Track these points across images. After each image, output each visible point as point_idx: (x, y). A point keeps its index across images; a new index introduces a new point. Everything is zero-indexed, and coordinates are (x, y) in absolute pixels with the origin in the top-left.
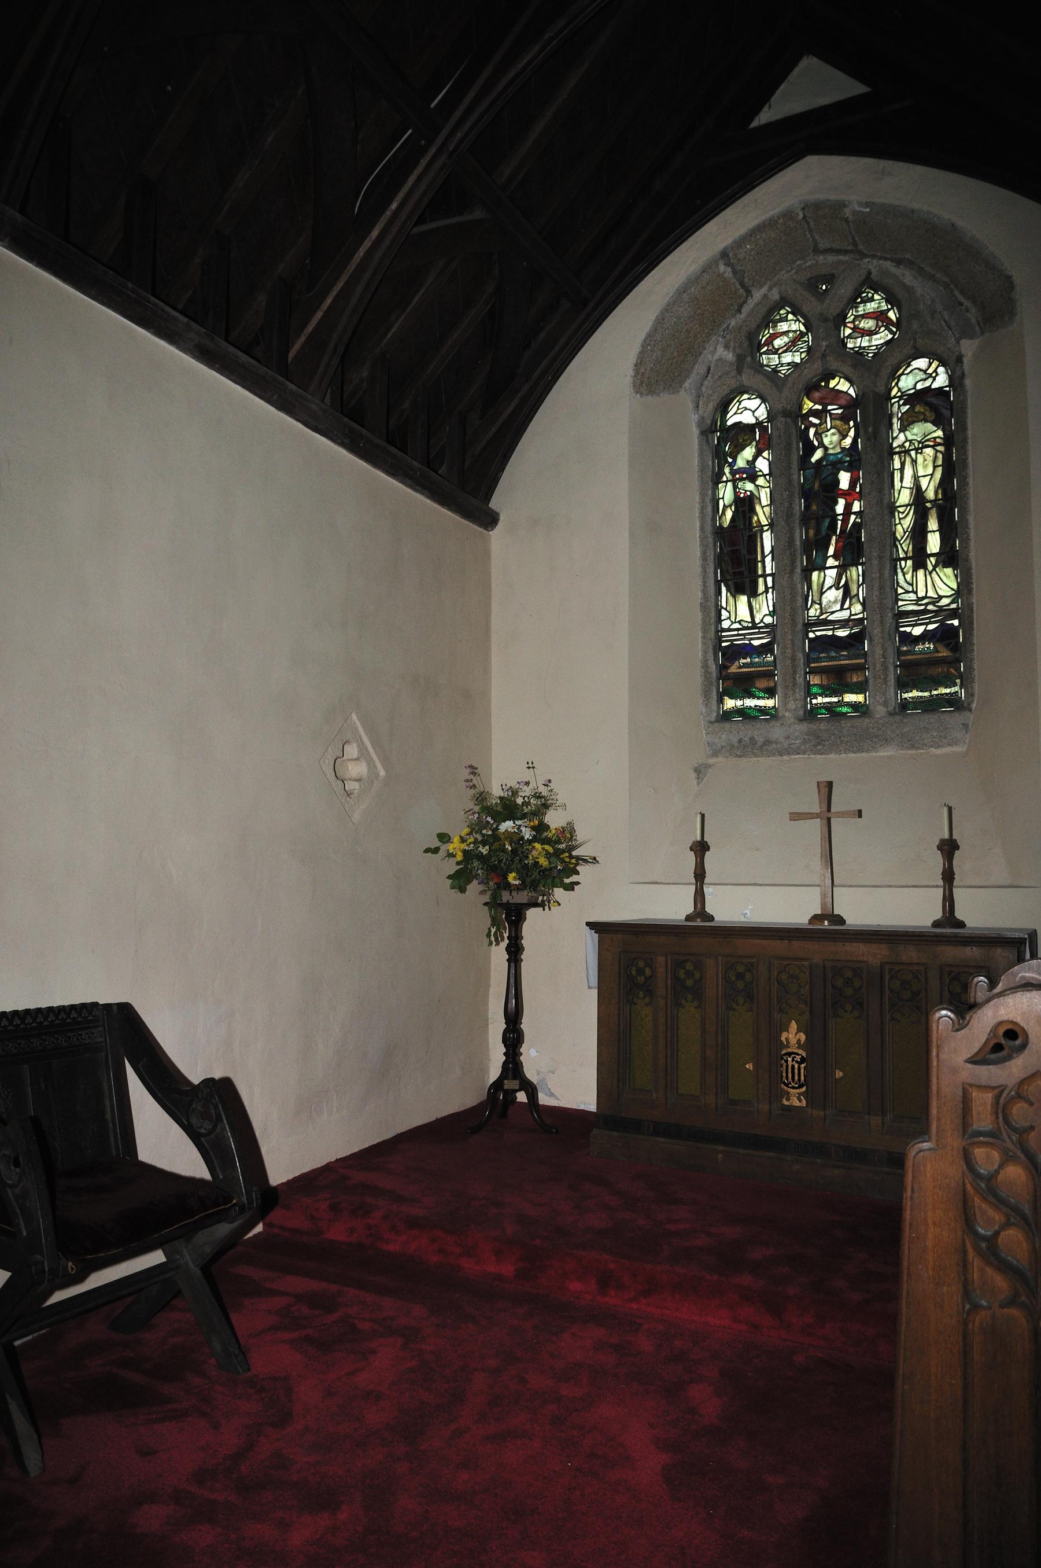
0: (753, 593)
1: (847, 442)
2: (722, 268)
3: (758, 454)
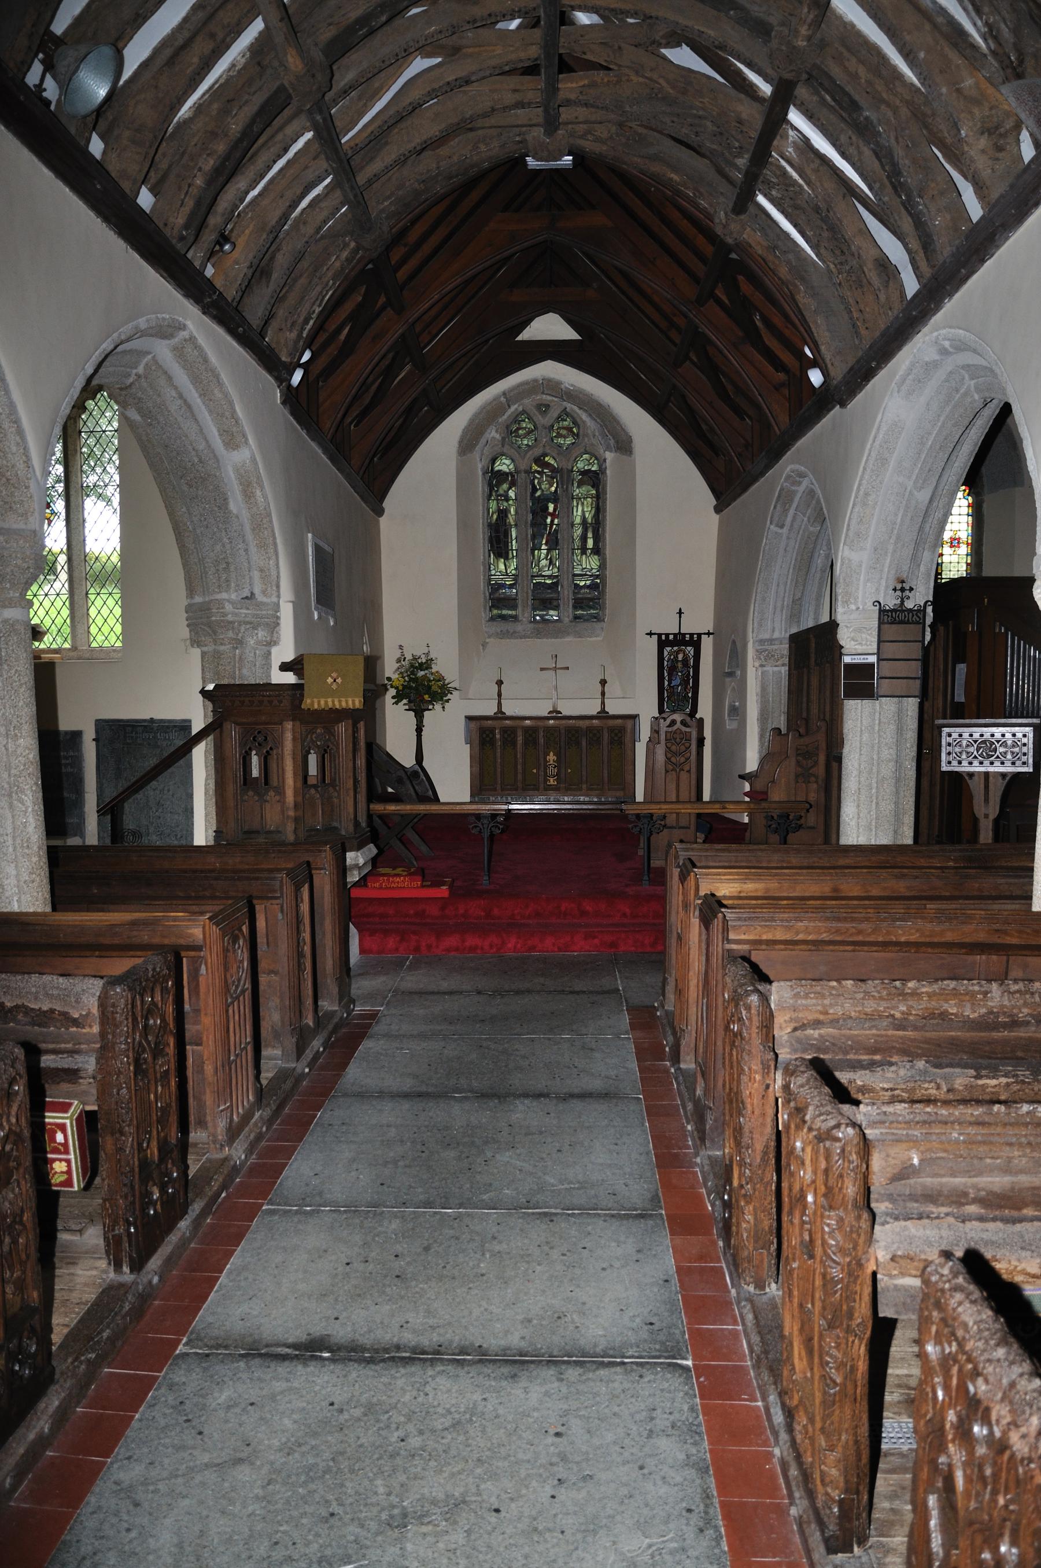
0: (506, 558)
1: (553, 489)
2: (502, 399)
3: (510, 488)
